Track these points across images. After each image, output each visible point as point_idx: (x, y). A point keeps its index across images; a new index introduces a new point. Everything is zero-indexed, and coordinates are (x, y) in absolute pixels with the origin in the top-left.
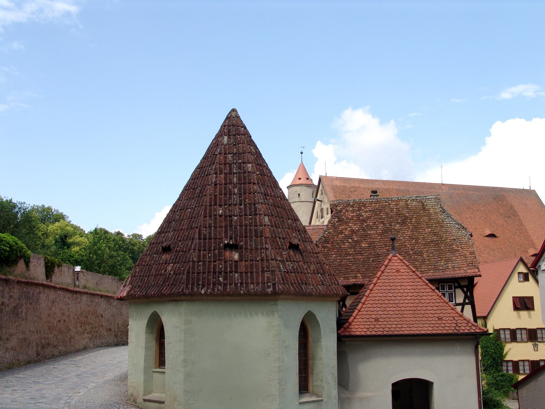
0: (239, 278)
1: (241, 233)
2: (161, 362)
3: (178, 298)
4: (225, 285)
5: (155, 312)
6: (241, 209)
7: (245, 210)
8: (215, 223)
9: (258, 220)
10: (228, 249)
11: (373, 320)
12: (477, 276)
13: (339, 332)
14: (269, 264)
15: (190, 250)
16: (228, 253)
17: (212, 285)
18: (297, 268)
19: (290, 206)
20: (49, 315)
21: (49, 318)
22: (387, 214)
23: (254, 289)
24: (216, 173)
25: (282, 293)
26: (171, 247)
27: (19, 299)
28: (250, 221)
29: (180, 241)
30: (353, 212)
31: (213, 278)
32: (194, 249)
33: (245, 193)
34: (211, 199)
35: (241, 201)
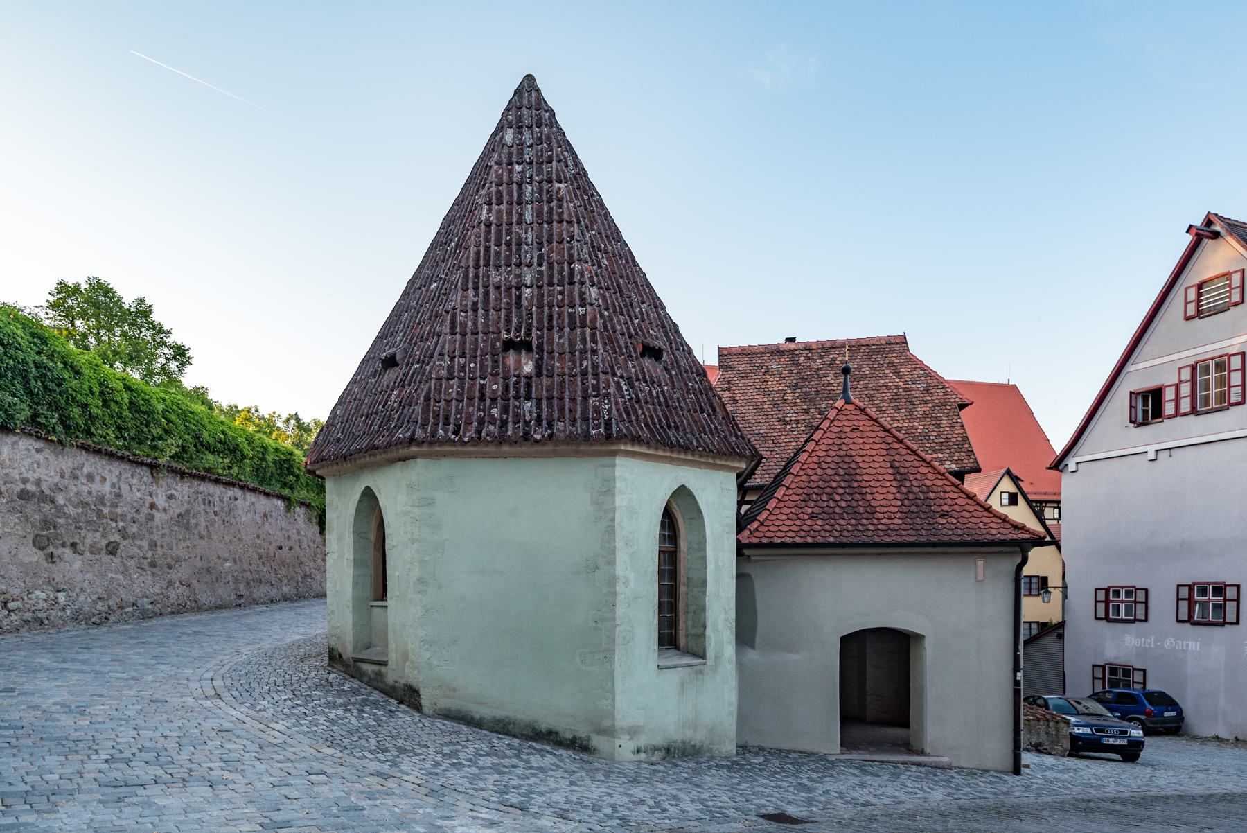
1: (540, 321)
2: (384, 596)
3: (403, 452)
4: (504, 424)
6: (540, 273)
7: (551, 277)
10: (511, 351)
12: (969, 472)
15: (431, 357)
16: (511, 358)
17: (475, 423)
18: (658, 396)
20: (258, 537)
23: (564, 431)
24: (489, 204)
25: (622, 438)
27: (189, 502)
28: (560, 297)
31: (479, 410)
32: (441, 354)
33: (550, 242)
34: (478, 253)
35: (540, 257)
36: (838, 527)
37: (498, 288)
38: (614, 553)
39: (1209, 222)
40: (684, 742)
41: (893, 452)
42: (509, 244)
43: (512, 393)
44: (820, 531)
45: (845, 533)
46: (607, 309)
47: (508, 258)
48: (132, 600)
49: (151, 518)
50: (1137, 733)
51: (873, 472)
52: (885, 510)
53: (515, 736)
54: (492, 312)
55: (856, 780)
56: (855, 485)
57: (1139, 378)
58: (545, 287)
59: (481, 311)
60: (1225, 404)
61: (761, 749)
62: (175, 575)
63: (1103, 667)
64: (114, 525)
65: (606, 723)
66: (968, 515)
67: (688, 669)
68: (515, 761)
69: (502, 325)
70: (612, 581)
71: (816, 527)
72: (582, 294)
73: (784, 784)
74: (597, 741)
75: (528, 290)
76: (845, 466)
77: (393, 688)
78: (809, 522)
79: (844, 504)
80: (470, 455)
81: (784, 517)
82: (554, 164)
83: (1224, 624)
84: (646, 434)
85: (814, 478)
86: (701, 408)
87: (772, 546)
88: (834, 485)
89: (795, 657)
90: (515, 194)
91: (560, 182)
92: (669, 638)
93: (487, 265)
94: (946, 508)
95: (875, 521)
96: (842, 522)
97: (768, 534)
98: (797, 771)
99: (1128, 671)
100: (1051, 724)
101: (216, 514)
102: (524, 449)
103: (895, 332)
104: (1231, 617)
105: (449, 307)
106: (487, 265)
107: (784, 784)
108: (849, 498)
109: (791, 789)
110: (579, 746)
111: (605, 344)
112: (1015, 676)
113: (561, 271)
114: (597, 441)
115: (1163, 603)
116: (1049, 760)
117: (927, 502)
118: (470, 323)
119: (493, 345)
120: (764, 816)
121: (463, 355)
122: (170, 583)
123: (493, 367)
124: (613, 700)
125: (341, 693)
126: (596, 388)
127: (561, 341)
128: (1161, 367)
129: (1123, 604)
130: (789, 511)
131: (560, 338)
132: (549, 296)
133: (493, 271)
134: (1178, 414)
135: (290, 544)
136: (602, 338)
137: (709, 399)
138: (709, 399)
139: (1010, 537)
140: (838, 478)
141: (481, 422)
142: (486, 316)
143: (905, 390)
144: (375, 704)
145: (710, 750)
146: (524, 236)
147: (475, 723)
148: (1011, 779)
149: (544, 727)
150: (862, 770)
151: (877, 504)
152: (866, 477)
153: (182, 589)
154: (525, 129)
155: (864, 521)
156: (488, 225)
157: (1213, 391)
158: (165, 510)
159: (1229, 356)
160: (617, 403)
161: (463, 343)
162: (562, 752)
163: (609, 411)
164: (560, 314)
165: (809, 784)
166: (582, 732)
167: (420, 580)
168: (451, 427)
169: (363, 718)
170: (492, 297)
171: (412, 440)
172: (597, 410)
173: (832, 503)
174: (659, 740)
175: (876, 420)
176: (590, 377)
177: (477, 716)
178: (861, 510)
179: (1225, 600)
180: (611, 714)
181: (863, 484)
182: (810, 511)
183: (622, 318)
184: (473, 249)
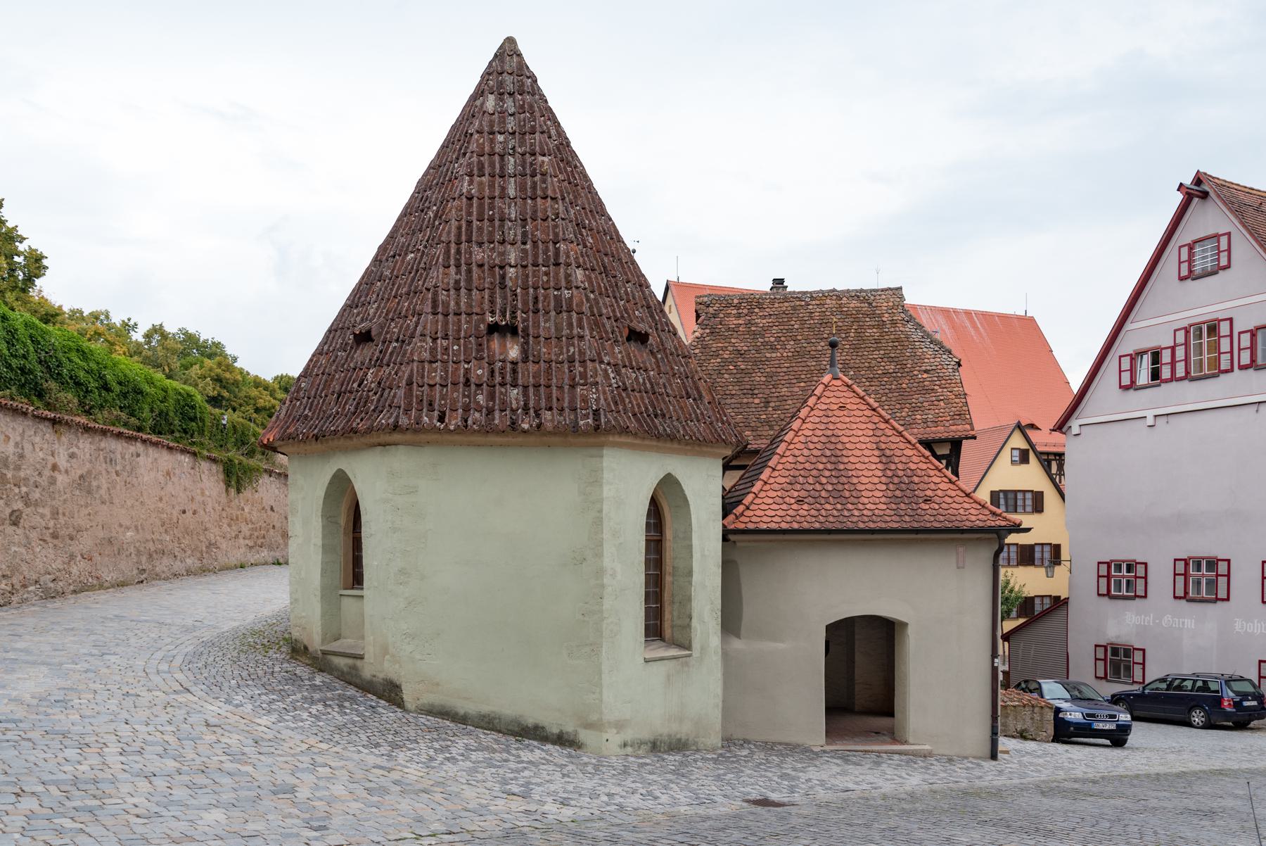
1: (525, 303)
2: (357, 579)
3: (388, 438)
4: (490, 412)
5: (340, 471)
7: (536, 256)
8: (469, 279)
9: (562, 275)
10: (496, 335)
11: (793, 501)
12: (967, 438)
13: (726, 522)
14: (585, 369)
15: (412, 337)
16: (496, 343)
17: (460, 411)
19: (632, 257)
20: (161, 499)
21: (161, 505)
22: (803, 322)
23: (552, 421)
24: (471, 175)
25: (610, 430)
26: (373, 333)
27: (91, 462)
28: (545, 278)
29: (393, 320)
30: (739, 316)
31: (464, 396)
34: (459, 228)
35: (524, 234)
36: (823, 512)
37: (481, 266)
38: (602, 545)
39: (1198, 180)
40: (670, 736)
41: (879, 433)
42: (491, 220)
43: (498, 379)
44: (806, 517)
45: (831, 519)
46: (592, 292)
47: (491, 233)
48: (34, 577)
49: (53, 481)
50: (1125, 717)
51: (858, 453)
52: (870, 494)
55: (838, 769)
56: (842, 467)
58: (530, 267)
59: (463, 291)
61: (746, 741)
62: (75, 548)
63: (1105, 647)
64: (17, 490)
65: (594, 717)
66: (950, 500)
67: (674, 661)
68: (505, 755)
69: (486, 306)
70: (600, 572)
71: (801, 512)
72: (568, 276)
73: (770, 774)
74: (584, 736)
75: (512, 270)
76: (832, 447)
77: (371, 683)
79: (830, 487)
80: (454, 444)
81: (771, 501)
82: (537, 135)
83: (1217, 599)
84: (633, 425)
85: (801, 459)
86: (687, 393)
87: (757, 532)
88: (821, 467)
89: (781, 646)
90: (497, 166)
92: (654, 630)
93: (469, 241)
94: (929, 493)
95: (861, 507)
96: (828, 507)
97: (754, 519)
98: (782, 762)
99: (1128, 652)
100: (1036, 710)
101: (117, 474)
104: (1140, 592)
105: (429, 284)
106: (469, 241)
107: (770, 774)
108: (835, 481)
109: (775, 778)
110: (562, 740)
111: (592, 330)
112: (993, 662)
113: (546, 251)
114: (586, 433)
115: (1161, 579)
116: (1030, 745)
117: (912, 486)
118: (452, 303)
119: (477, 327)
120: (748, 801)
121: (446, 337)
122: (72, 557)
123: (478, 351)
124: (601, 693)
125: (314, 688)
126: (583, 375)
127: (546, 325)
129: (1122, 580)
130: (774, 494)
131: (546, 322)
132: (534, 276)
133: (475, 248)
135: (194, 507)
136: (589, 323)
137: (694, 383)
138: (694, 383)
139: (989, 523)
140: (824, 460)
141: (467, 409)
144: (352, 699)
145: (695, 743)
146: (507, 211)
147: (462, 720)
148: (989, 765)
149: (530, 721)
150: (846, 760)
151: (863, 487)
152: (852, 459)
153: (83, 564)
154: (506, 96)
155: (850, 506)
156: (470, 199)
158: (67, 472)
160: (604, 393)
161: (446, 323)
162: (549, 746)
163: (597, 400)
164: (546, 297)
165: (793, 773)
166: (569, 728)
167: (402, 571)
168: (436, 413)
169: (346, 714)
170: (475, 276)
171: (396, 427)
172: (585, 400)
173: (818, 487)
174: (646, 735)
175: (862, 398)
176: (577, 364)
177: (462, 712)
178: (847, 494)
179: (1217, 575)
181: (850, 466)
182: (796, 494)
183: (607, 299)
184: (454, 223)
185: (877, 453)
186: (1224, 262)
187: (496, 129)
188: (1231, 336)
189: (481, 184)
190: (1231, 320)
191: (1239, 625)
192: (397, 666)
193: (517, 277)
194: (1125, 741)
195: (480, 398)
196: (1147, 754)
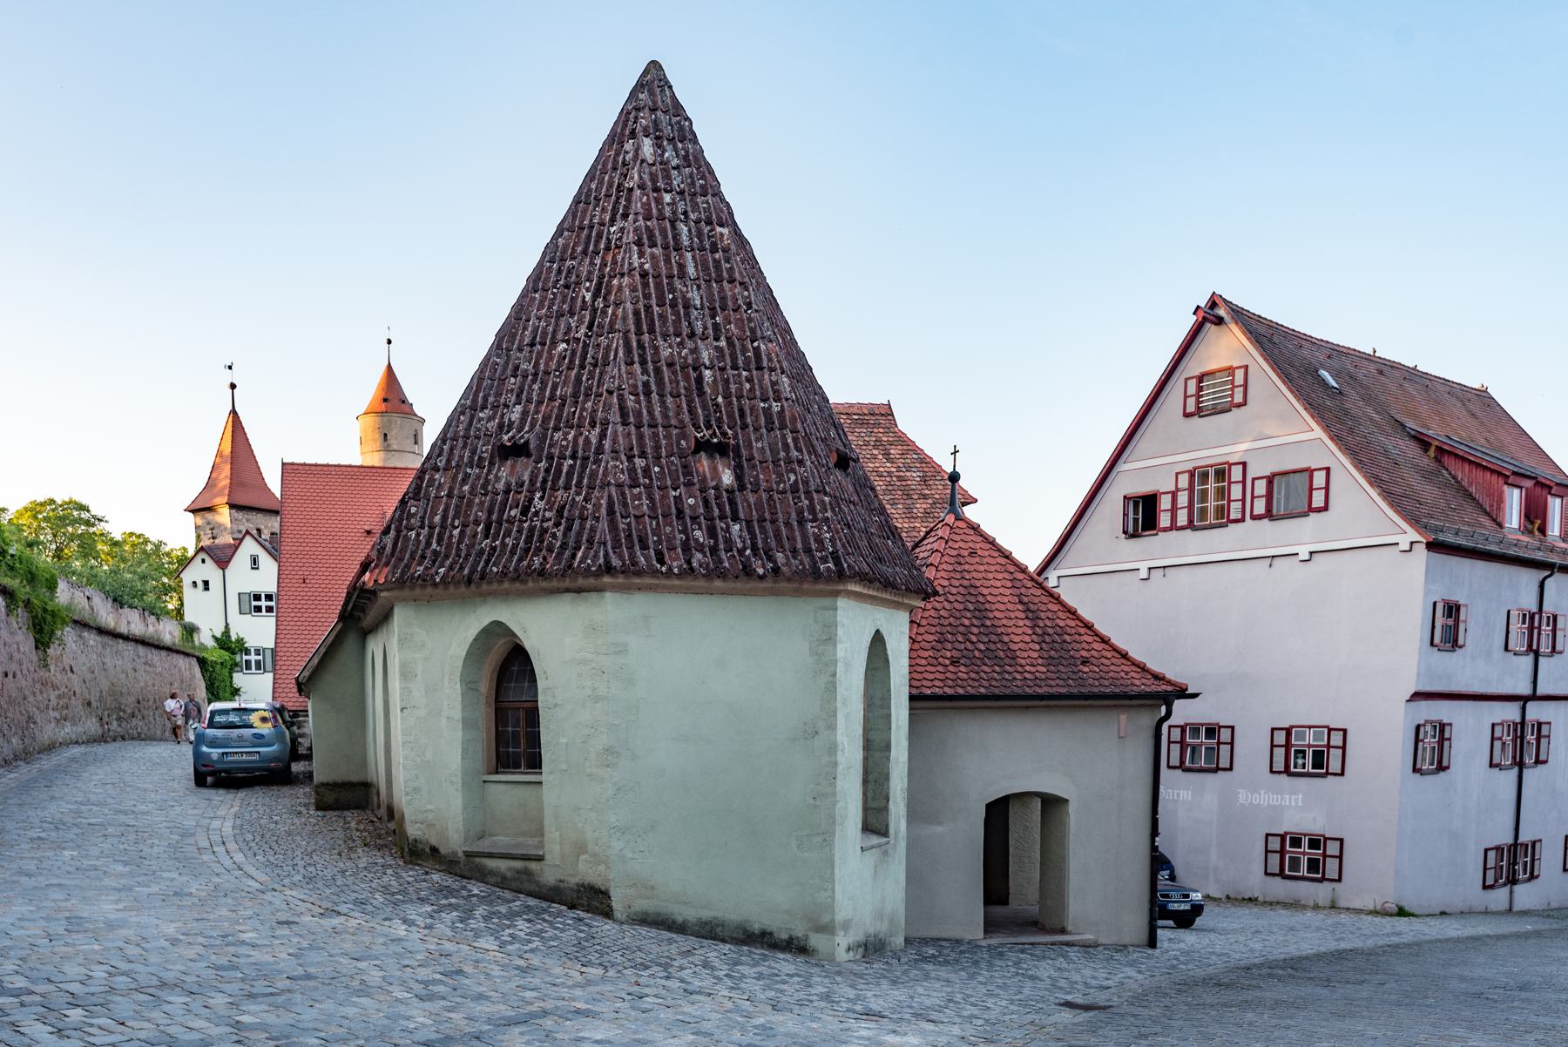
0: (745, 533)
1: (731, 416)
3: (581, 582)
5: (497, 630)
16: (704, 463)
24: (639, 243)
35: (716, 326)
37: (670, 365)
39: (1213, 304)
42: (673, 305)
53: (723, 941)
54: (669, 400)
57: (1132, 480)
59: (655, 397)
60: (1223, 519)
65: (826, 919)
74: (816, 940)
78: (951, 668)
83: (1217, 770)
88: (967, 622)
89: (939, 829)
91: (721, 225)
93: (652, 331)
94: (1084, 653)
102: (739, 585)
103: (879, 399)
104: (1224, 763)
110: (796, 947)
115: (1252, 748)
124: (833, 891)
126: (812, 509)
128: (1151, 472)
130: (926, 654)
134: (1173, 527)
140: (968, 615)
142: (663, 403)
143: (900, 478)
147: (681, 928)
149: (756, 928)
152: (998, 614)
156: (644, 275)
157: (1211, 504)
159: (1230, 465)
161: (641, 437)
166: (799, 932)
167: (609, 750)
177: (680, 919)
178: (1001, 654)
179: (1219, 743)
180: (830, 907)
181: (996, 622)
182: (948, 654)
185: (1020, 607)
186: (1238, 398)
187: (660, 184)
188: (1244, 482)
189: (653, 256)
190: (1244, 464)
191: (1243, 796)
192: (602, 867)
193: (715, 381)
194: (1192, 922)
195: (698, 533)
196: (1212, 936)
